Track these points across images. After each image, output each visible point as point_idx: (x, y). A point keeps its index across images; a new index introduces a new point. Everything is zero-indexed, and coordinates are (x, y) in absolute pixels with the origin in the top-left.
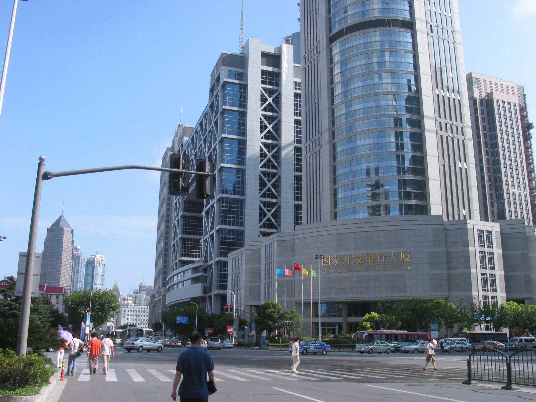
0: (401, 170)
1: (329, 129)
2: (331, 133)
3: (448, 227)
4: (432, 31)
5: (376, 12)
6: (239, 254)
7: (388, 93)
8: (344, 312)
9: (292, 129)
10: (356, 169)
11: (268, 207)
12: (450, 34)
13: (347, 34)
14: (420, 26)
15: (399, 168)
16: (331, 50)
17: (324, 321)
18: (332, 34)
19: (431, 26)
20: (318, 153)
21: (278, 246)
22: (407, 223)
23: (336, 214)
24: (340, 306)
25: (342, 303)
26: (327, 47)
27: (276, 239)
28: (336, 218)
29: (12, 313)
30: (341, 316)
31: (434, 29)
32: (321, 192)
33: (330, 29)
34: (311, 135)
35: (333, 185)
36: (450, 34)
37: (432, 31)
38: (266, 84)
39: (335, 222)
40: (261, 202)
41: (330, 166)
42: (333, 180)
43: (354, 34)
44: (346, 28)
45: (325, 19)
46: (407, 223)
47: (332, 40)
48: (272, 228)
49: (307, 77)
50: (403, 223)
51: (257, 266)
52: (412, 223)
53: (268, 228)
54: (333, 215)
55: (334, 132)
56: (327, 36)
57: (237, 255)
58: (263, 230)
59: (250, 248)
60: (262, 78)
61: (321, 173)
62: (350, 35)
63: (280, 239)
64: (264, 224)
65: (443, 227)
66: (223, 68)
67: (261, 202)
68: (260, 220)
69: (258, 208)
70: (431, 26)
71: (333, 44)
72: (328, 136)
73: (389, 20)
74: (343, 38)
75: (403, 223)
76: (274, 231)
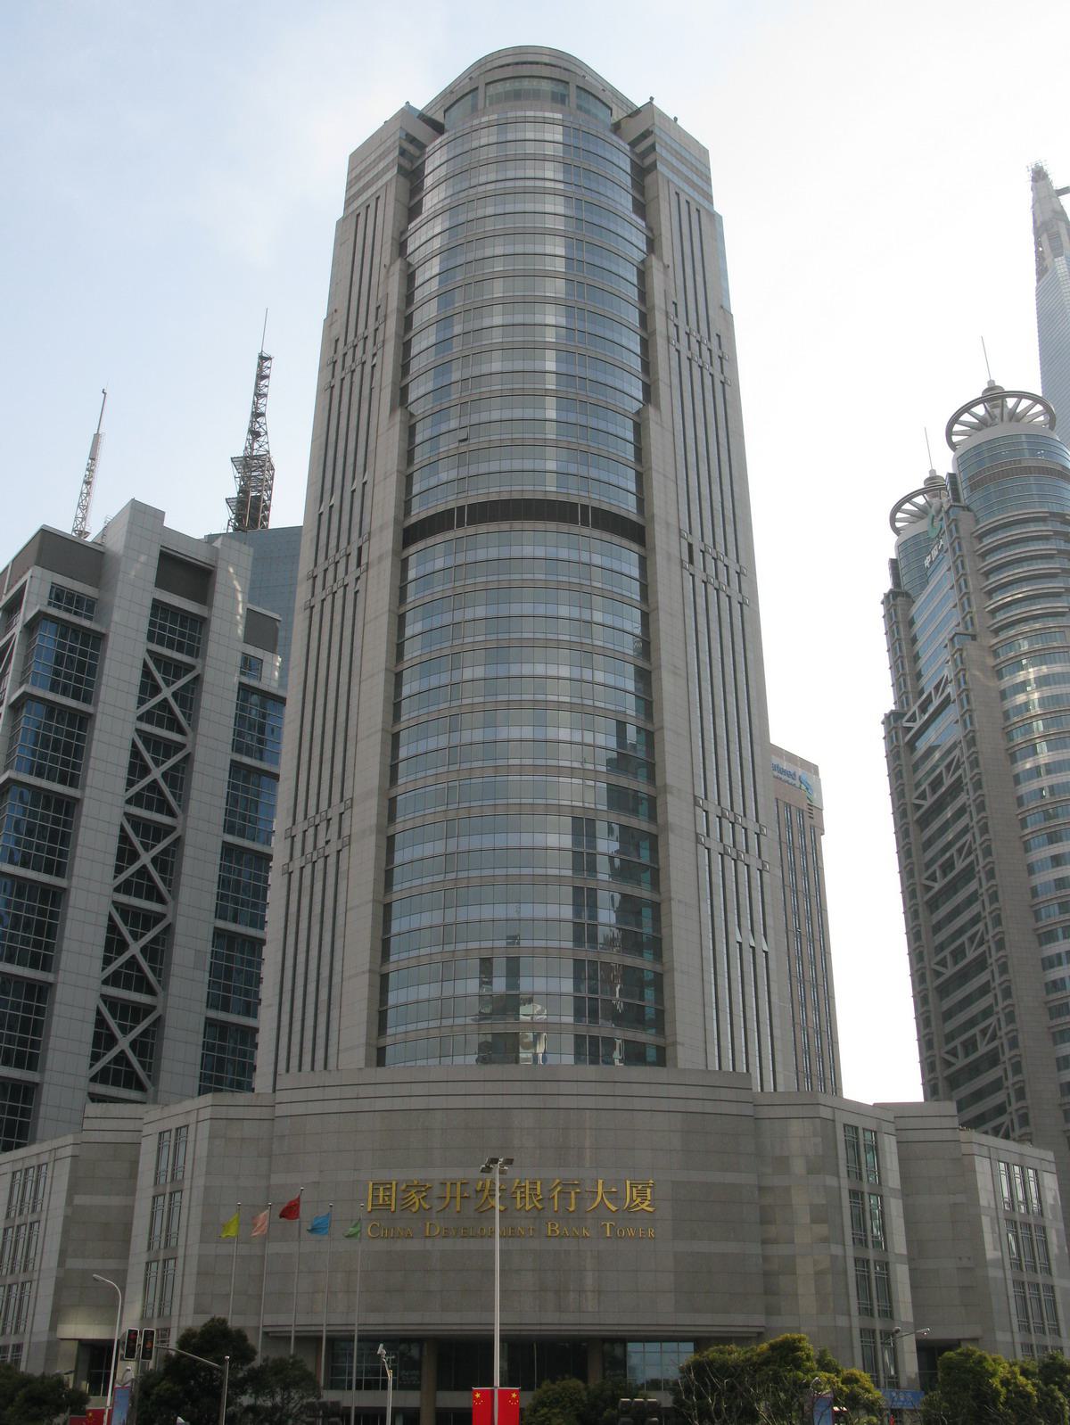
0: (584, 933)
1: (382, 792)
2: (386, 803)
3: (765, 1112)
4: (691, 561)
5: (551, 478)
6: (45, 1158)
7: (559, 706)
8: (428, 1373)
9: (223, 789)
10: (462, 918)
11: (124, 1018)
12: (734, 577)
13: (460, 524)
14: (665, 541)
15: (578, 927)
16: (404, 565)
17: (401, 1404)
18: (413, 520)
19: (690, 546)
20: (331, 860)
21: (212, 1137)
22: (645, 1090)
23: (381, 1052)
24: (415, 1352)
25: (419, 1340)
26: (395, 553)
27: (206, 1113)
28: (381, 1061)
29: (308, 1403)
30: (417, 1387)
31: (698, 556)
32: (336, 979)
33: (406, 505)
34: (312, 801)
35: (379, 961)
36: (734, 577)
37: (691, 561)
38: (160, 643)
39: (381, 1074)
40: (104, 998)
41: (374, 901)
42: (379, 948)
43: (483, 528)
44: (461, 509)
45: (394, 477)
46: (645, 1090)
47: (411, 535)
48: (127, 1085)
49: (315, 635)
50: (636, 1089)
51: (116, 1201)
52: (663, 1091)
53: (116, 1083)
54: (375, 1053)
55: (393, 801)
56: (396, 521)
57: (34, 1162)
58: (100, 1089)
59: (96, 1137)
60: (152, 623)
61: (340, 921)
62: (471, 530)
63: (223, 1112)
64: (105, 1070)
65: (748, 1110)
66: (37, 571)
67: (104, 998)
68: (95, 1057)
69: (92, 1017)
70: (690, 546)
71: (413, 549)
72: (374, 811)
73: (585, 507)
74: (449, 535)
75: (636, 1089)
76: (134, 1095)
